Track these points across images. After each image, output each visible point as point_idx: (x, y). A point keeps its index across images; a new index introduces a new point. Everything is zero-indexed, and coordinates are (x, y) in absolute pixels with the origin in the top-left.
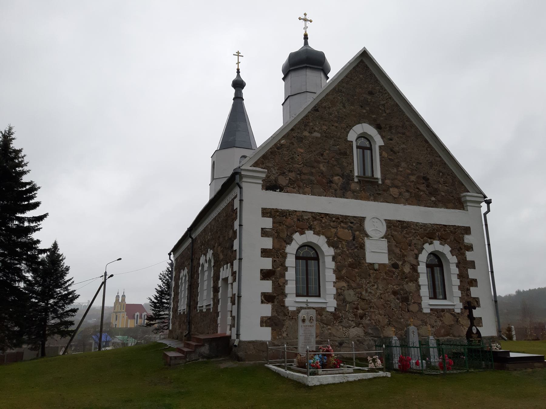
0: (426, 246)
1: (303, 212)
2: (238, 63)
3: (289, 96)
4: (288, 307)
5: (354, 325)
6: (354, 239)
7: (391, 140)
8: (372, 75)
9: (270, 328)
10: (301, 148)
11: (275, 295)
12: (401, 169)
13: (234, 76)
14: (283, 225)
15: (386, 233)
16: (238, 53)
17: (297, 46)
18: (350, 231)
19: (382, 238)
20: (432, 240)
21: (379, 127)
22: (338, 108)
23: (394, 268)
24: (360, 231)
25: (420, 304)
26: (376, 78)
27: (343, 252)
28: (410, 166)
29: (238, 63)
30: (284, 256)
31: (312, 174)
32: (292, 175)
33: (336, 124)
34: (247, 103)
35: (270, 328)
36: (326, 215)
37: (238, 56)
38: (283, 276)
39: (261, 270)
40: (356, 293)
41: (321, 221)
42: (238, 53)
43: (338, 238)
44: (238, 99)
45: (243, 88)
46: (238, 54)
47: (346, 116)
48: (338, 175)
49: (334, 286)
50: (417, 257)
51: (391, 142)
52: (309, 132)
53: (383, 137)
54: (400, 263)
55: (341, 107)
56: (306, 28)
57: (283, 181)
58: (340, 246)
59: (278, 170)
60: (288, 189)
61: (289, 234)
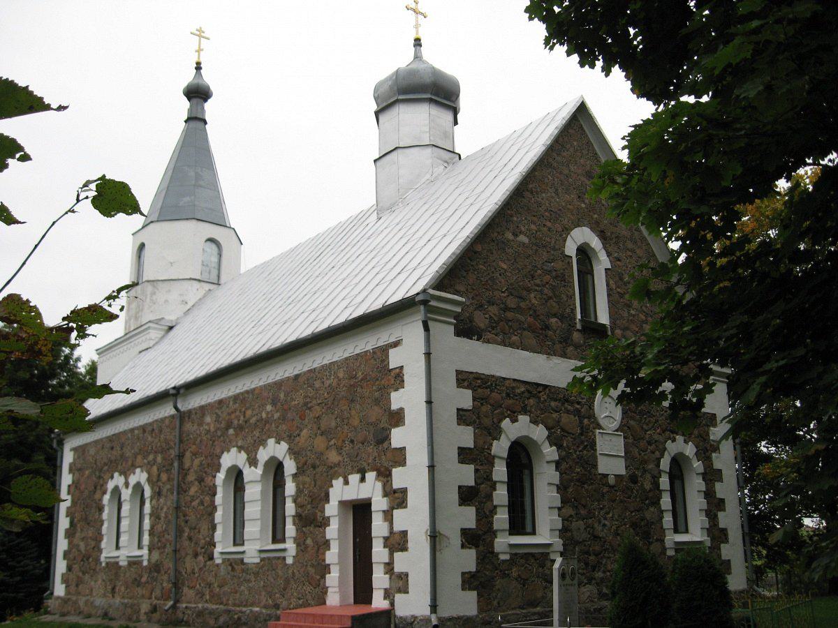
0: (669, 444)
1: (514, 380)
2: (199, 51)
3: (396, 148)
4: (498, 554)
5: (585, 581)
6: (582, 434)
7: (619, 260)
8: (589, 143)
9: (475, 593)
10: (503, 261)
11: (480, 532)
12: (633, 312)
13: (188, 77)
14: (489, 400)
15: (622, 422)
16: (200, 30)
17: (402, 59)
18: (577, 418)
19: (617, 430)
20: (675, 435)
21: (602, 236)
22: (549, 194)
23: (633, 483)
24: (589, 418)
25: (662, 541)
26: (594, 149)
27: (569, 454)
28: (644, 308)
29: (199, 51)
30: (490, 461)
31: (518, 309)
32: (493, 310)
33: (549, 224)
34: (213, 131)
35: (475, 593)
36: (546, 387)
37: (200, 36)
38: (489, 497)
39: (460, 487)
40: (588, 527)
41: (539, 398)
42: (200, 30)
43: (563, 430)
44: (196, 120)
45: (206, 100)
46: (200, 34)
47: (560, 210)
48: (555, 315)
49: (559, 516)
50: (658, 465)
51: (618, 263)
52: (513, 234)
53: (609, 254)
54: (639, 473)
55: (553, 195)
56: (417, 26)
57: (481, 320)
58: (565, 445)
59: (473, 298)
60: (490, 336)
61: (495, 420)
